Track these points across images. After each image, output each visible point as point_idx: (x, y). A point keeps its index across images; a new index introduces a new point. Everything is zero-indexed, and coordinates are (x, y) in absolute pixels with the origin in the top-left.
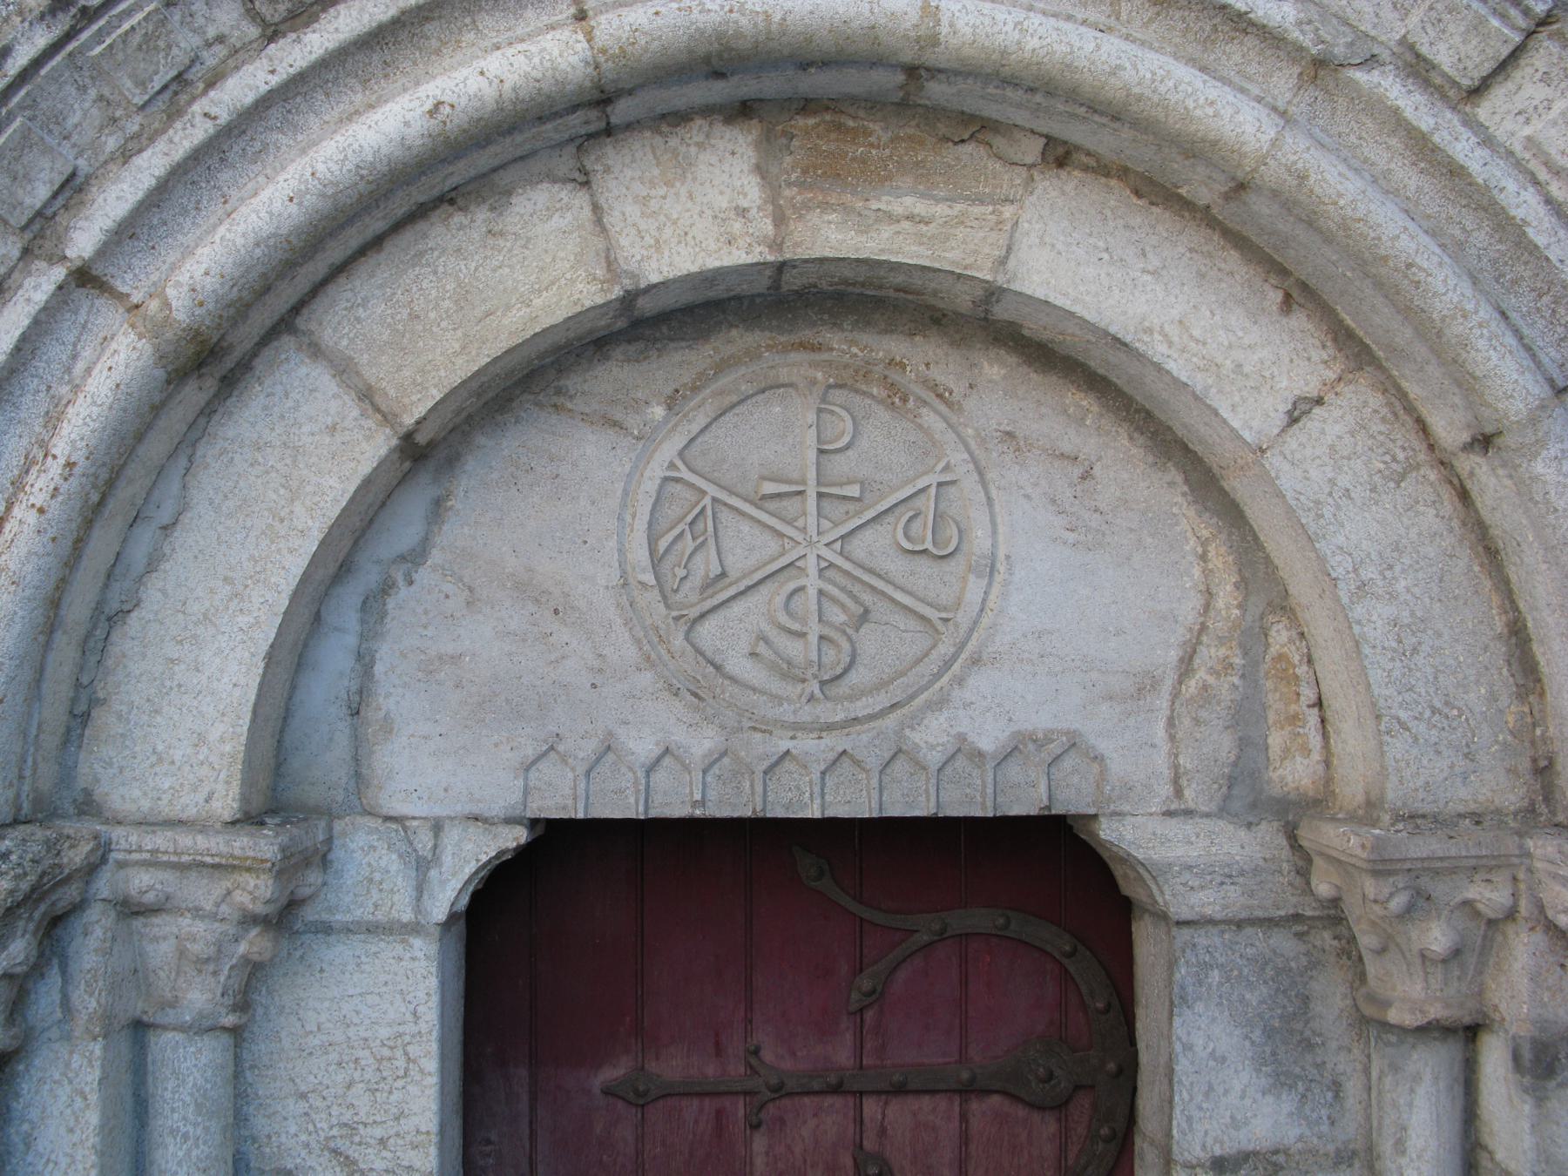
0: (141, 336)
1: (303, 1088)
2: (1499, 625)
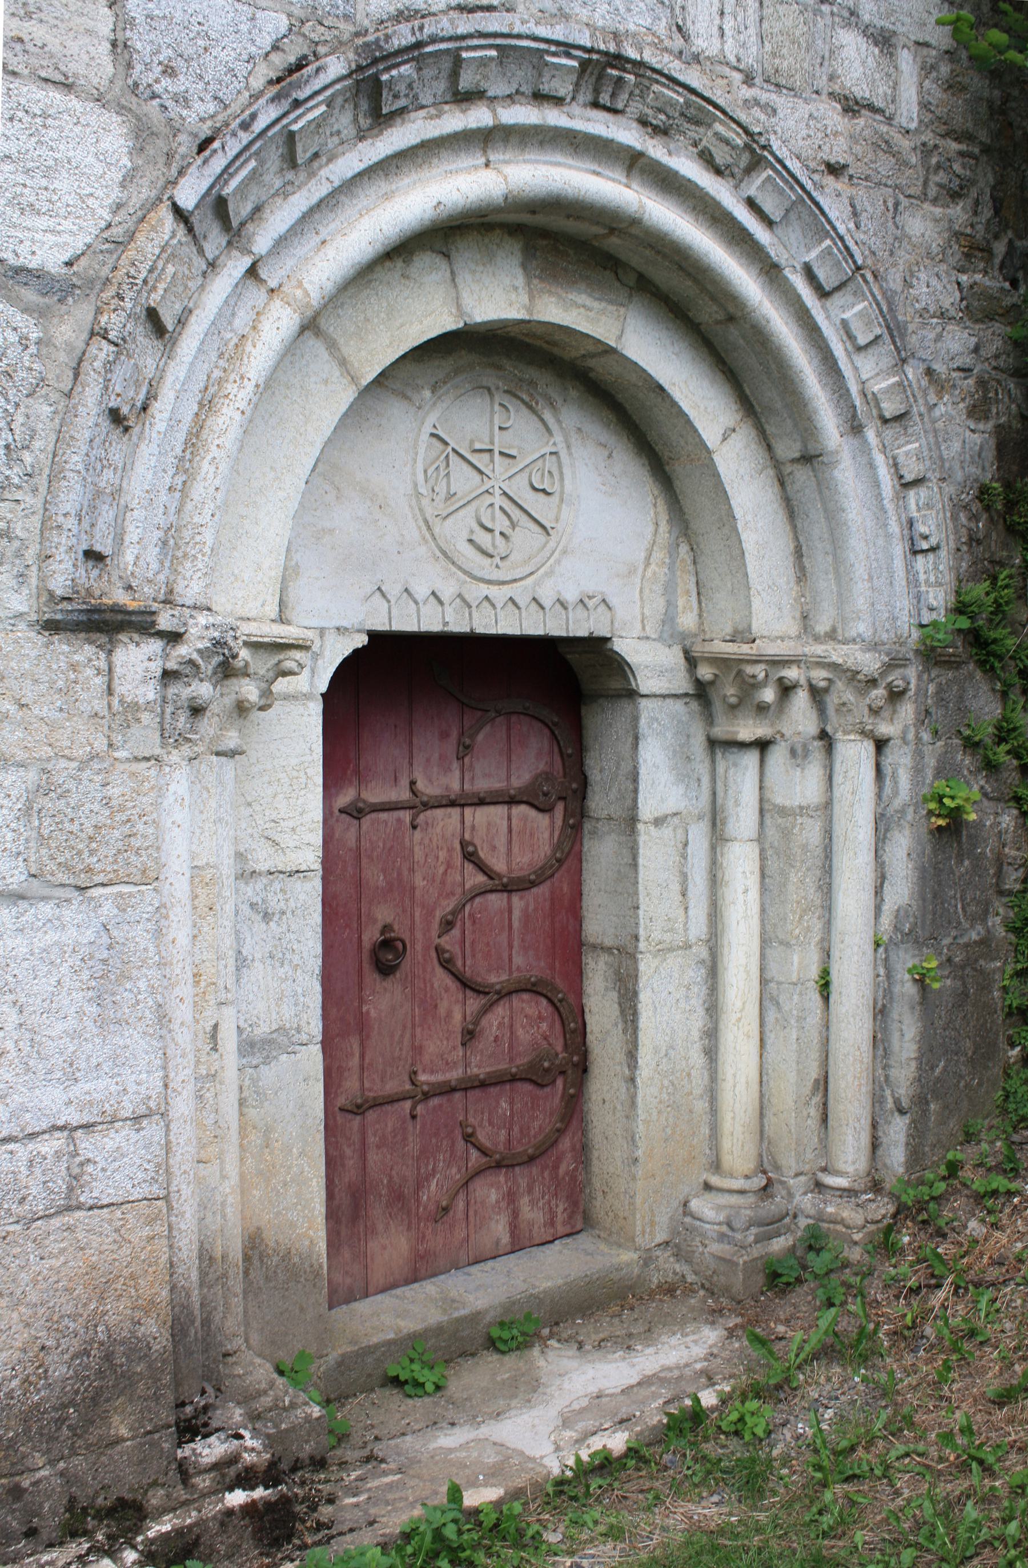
0: (295, 311)
1: (249, 799)
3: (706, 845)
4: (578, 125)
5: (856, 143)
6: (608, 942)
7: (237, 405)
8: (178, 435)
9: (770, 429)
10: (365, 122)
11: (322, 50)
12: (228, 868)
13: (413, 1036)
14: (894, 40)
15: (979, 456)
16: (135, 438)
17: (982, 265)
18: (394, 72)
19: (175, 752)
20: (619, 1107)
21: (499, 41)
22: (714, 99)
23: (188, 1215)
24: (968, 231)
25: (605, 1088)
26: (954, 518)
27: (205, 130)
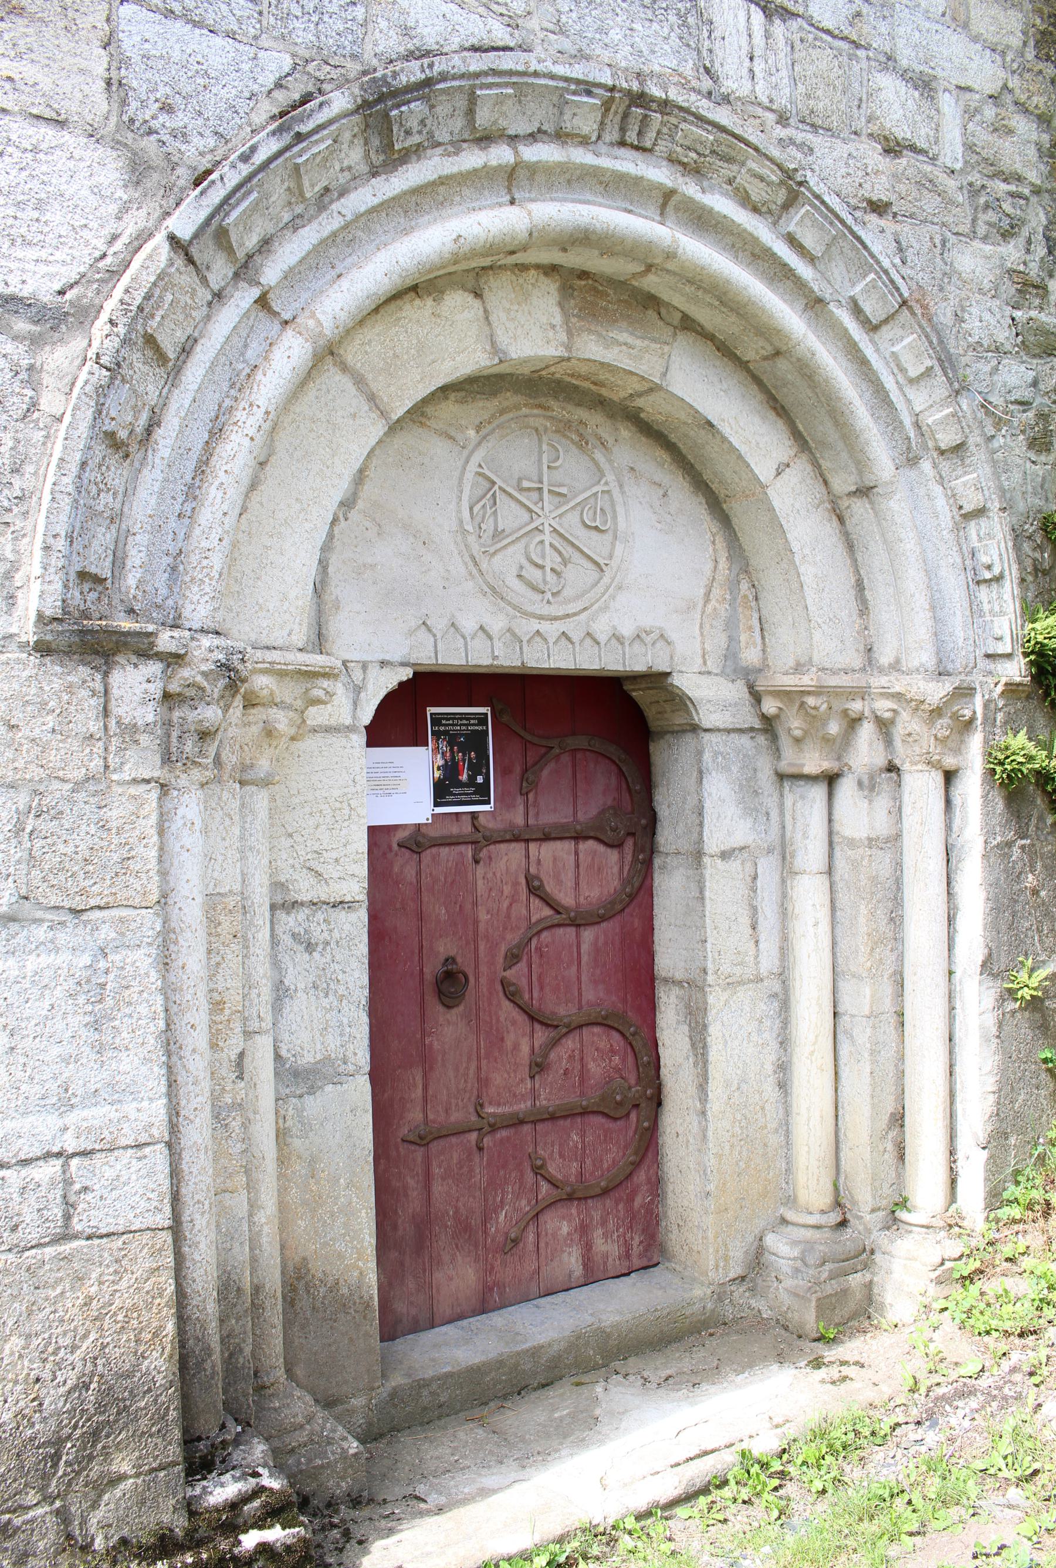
0: (307, 341)
1: (290, 831)
2: (853, 580)
3: (777, 878)
4: (605, 162)
5: (900, 181)
6: (679, 976)
7: (246, 432)
8: (188, 463)
9: (825, 464)
10: (378, 159)
11: (326, 87)
12: (260, 897)
13: (479, 1068)
14: (934, 84)
15: (1042, 487)
16: (137, 464)
17: (1037, 302)
18: (404, 108)
19: (184, 776)
20: (691, 1140)
21: (514, 79)
22: (746, 136)
23: (202, 1246)
24: (1021, 268)
25: (679, 1121)
26: (1017, 548)
27: (205, 164)
